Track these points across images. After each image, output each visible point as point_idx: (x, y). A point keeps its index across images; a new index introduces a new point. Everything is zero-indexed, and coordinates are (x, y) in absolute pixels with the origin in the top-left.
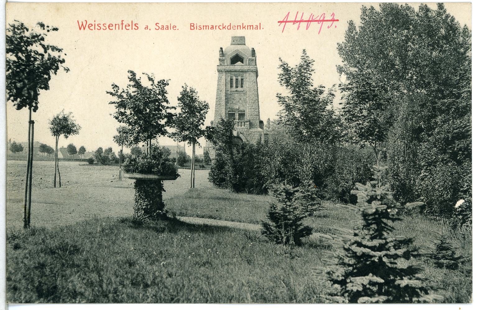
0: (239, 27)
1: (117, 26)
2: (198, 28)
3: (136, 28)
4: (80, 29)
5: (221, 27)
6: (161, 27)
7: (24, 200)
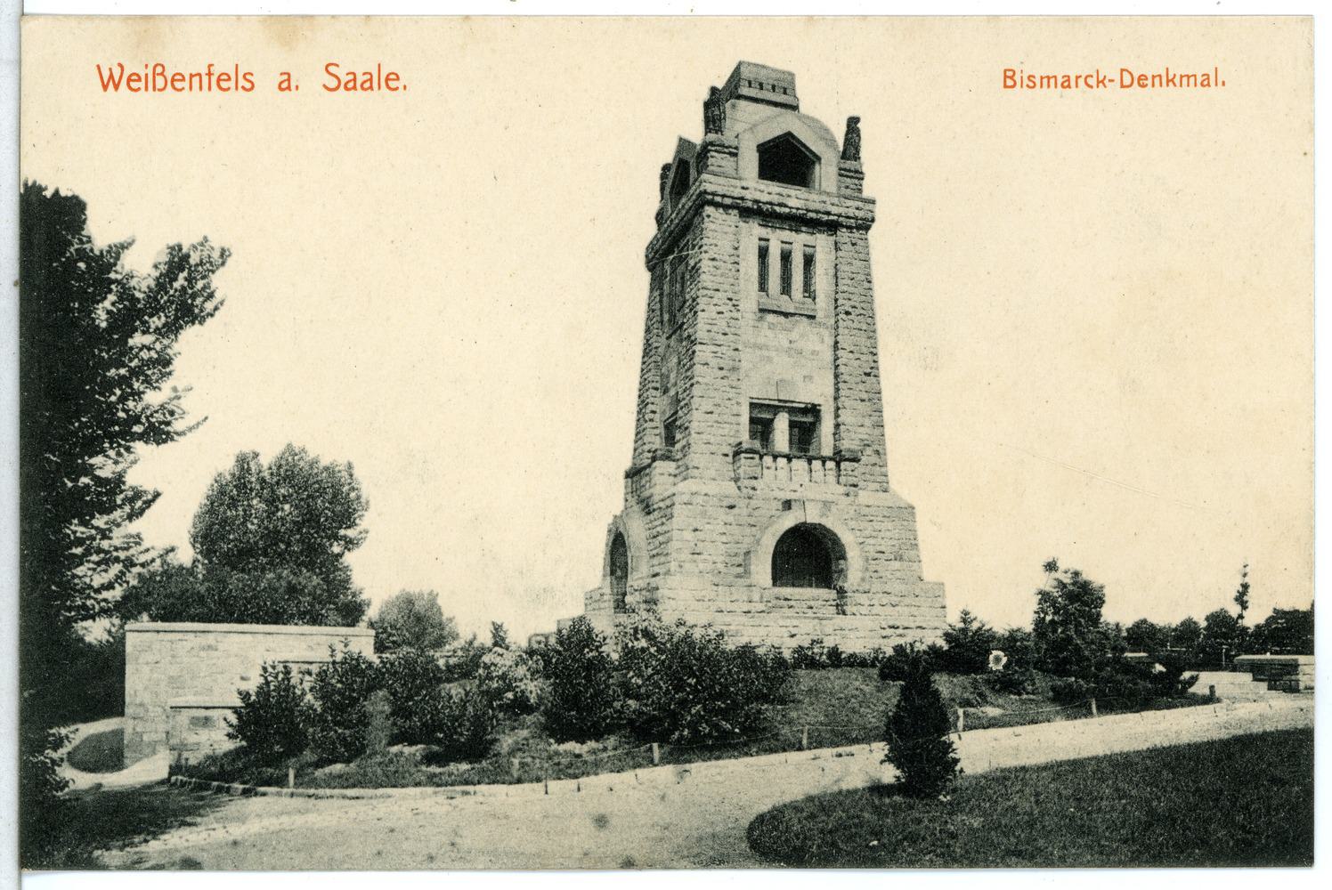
0: (1157, 81)
1: (196, 79)
2: (1026, 81)
3: (248, 85)
4: (105, 87)
5: (1092, 81)
6: (344, 79)
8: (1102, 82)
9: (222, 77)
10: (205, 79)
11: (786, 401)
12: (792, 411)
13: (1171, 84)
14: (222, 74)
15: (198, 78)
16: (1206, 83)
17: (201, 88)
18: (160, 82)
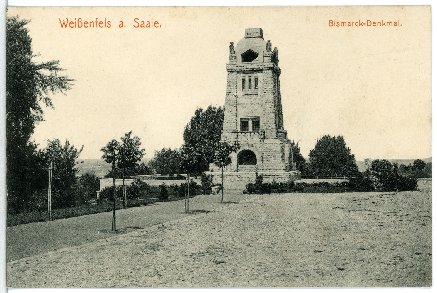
1: (92, 24)
3: (109, 26)
4: (62, 26)
5: (358, 24)
6: (140, 24)
7: (117, 220)
8: (361, 24)
9: (71, 23)
10: (95, 23)
11: (250, 117)
12: (252, 119)
13: (384, 25)
14: (100, 22)
15: (92, 23)
16: (395, 25)
17: (93, 27)
18: (80, 24)
